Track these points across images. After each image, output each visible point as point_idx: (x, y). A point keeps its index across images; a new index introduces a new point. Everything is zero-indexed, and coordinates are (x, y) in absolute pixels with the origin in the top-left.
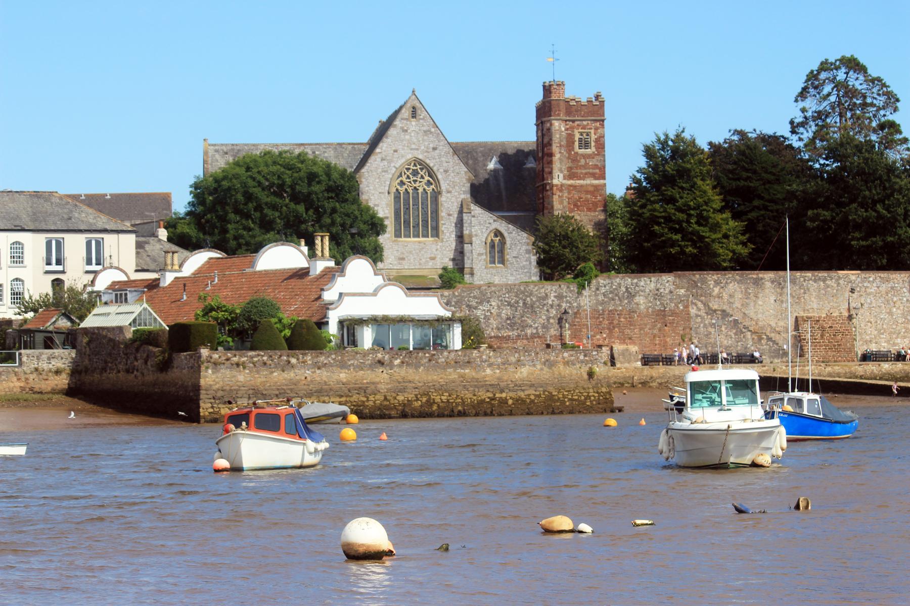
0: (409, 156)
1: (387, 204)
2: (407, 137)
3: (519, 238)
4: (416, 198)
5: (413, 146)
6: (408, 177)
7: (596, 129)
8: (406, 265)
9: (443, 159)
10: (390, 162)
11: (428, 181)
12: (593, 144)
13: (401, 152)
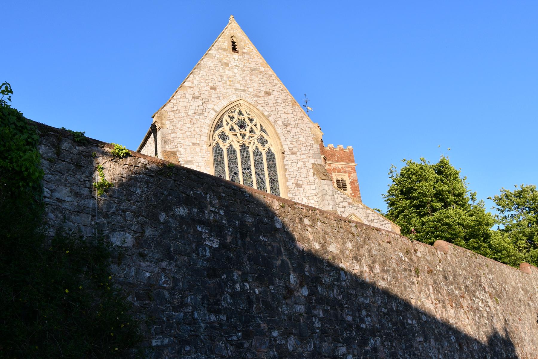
0: (234, 98)
2: (229, 73)
5: (238, 86)
6: (232, 129)
8: (189, 94)
9: (280, 108)
10: (206, 102)
12: (348, 186)
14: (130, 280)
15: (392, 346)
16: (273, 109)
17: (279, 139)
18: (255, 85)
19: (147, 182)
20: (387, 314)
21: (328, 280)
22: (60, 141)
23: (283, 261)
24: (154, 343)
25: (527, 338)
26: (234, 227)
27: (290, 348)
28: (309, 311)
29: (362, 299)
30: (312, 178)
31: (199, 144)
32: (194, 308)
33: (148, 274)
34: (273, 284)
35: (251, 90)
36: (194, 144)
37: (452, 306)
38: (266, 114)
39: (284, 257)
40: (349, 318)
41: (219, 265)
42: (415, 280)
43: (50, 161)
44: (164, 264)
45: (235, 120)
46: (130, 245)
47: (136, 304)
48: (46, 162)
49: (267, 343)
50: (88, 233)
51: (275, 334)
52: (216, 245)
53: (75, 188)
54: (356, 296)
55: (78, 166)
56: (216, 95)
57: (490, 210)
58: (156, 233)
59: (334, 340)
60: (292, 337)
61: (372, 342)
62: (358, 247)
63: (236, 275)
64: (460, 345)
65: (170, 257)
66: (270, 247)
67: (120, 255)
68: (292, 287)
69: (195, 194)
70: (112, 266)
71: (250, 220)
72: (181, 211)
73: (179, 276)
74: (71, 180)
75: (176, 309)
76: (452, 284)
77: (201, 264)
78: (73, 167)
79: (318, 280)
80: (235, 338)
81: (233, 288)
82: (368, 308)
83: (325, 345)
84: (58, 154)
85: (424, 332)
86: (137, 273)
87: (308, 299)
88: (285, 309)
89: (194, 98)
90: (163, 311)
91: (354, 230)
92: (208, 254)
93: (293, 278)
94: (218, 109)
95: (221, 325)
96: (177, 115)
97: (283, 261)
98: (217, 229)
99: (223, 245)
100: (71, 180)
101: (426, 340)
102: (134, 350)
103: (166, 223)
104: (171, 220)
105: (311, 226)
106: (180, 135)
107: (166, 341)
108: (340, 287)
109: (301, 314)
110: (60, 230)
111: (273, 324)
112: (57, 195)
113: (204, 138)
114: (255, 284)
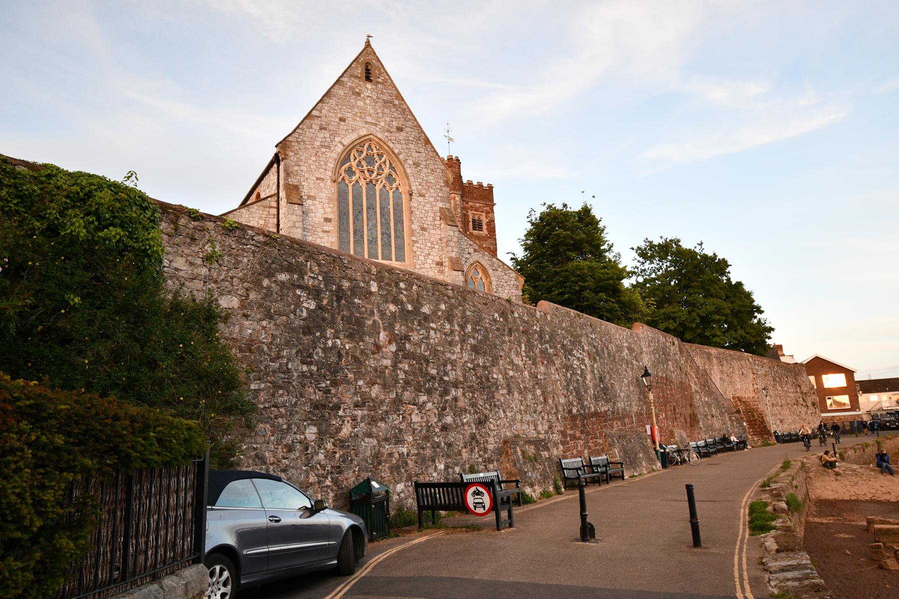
0: (363, 132)
1: (330, 199)
2: (360, 103)
3: (506, 277)
4: (371, 196)
5: (369, 119)
7: (487, 213)
10: (334, 134)
11: (390, 175)
12: (485, 227)
13: (350, 121)
14: (234, 336)
15: (473, 397)
16: (405, 146)
17: (408, 179)
18: (388, 119)
19: (254, 252)
20: (473, 369)
21: (416, 338)
22: (178, 218)
23: (374, 321)
24: (252, 387)
25: (622, 394)
26: (331, 291)
27: (374, 395)
28: (395, 365)
29: (448, 355)
30: (438, 222)
31: (323, 179)
32: (289, 360)
33: (250, 331)
34: (363, 341)
35: (382, 124)
36: (318, 179)
37: (543, 363)
38: (396, 151)
39: (376, 318)
40: (434, 372)
41: (314, 325)
42: (507, 339)
43: (169, 236)
44: (264, 323)
45: (363, 156)
46: (236, 307)
47: (238, 355)
48: (165, 236)
49: (353, 390)
50: (200, 297)
51: (361, 383)
52: (312, 307)
53: (190, 258)
54: (443, 353)
55: (193, 239)
56: (345, 128)
57: (628, 260)
58: (259, 297)
59: (416, 390)
60: (376, 386)
61: (454, 393)
62: (451, 308)
63: (329, 332)
64: (545, 399)
65: (271, 318)
66: (363, 309)
67: (226, 318)
68: (381, 343)
69: (296, 262)
70: (220, 324)
71: (346, 284)
72: (283, 277)
73: (277, 333)
74: (187, 251)
75: (272, 360)
76: (546, 342)
77: (297, 323)
78: (188, 240)
79: (407, 338)
80: (324, 385)
81: (325, 344)
82: (453, 363)
83: (407, 394)
84: (176, 229)
85: (508, 385)
86: (240, 331)
87: (395, 354)
88: (372, 363)
89: (321, 129)
90: (261, 362)
91: (450, 293)
92: (305, 314)
93: (383, 336)
94: (346, 142)
95: (312, 374)
96: (302, 146)
97: (374, 321)
98: (315, 293)
99: (319, 307)
100: (187, 251)
101: (510, 392)
102: (235, 392)
103: (269, 288)
104: (273, 285)
105: (406, 289)
106: (304, 169)
107: (263, 386)
108: (428, 344)
109: (386, 367)
110: (176, 294)
111: (359, 375)
112: (174, 265)
113: (329, 173)
114: (346, 340)
